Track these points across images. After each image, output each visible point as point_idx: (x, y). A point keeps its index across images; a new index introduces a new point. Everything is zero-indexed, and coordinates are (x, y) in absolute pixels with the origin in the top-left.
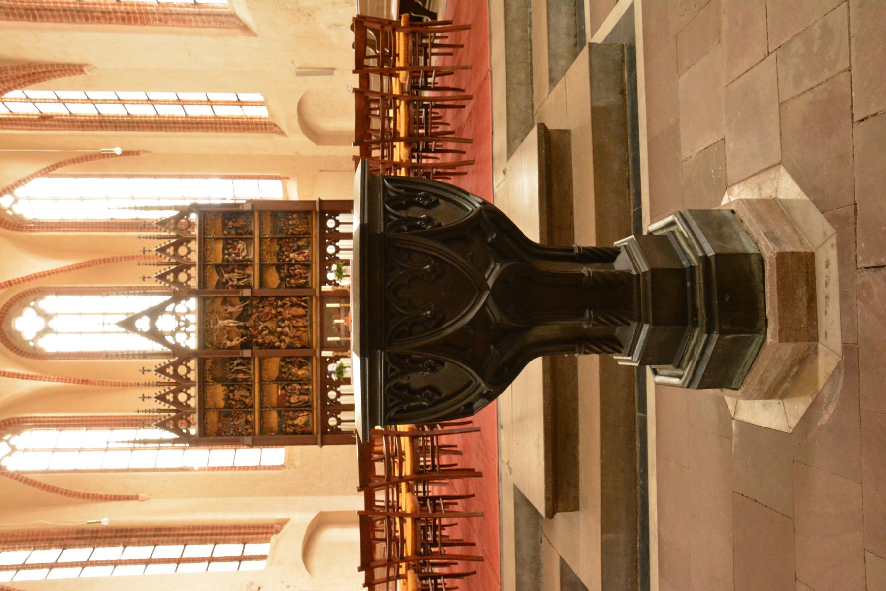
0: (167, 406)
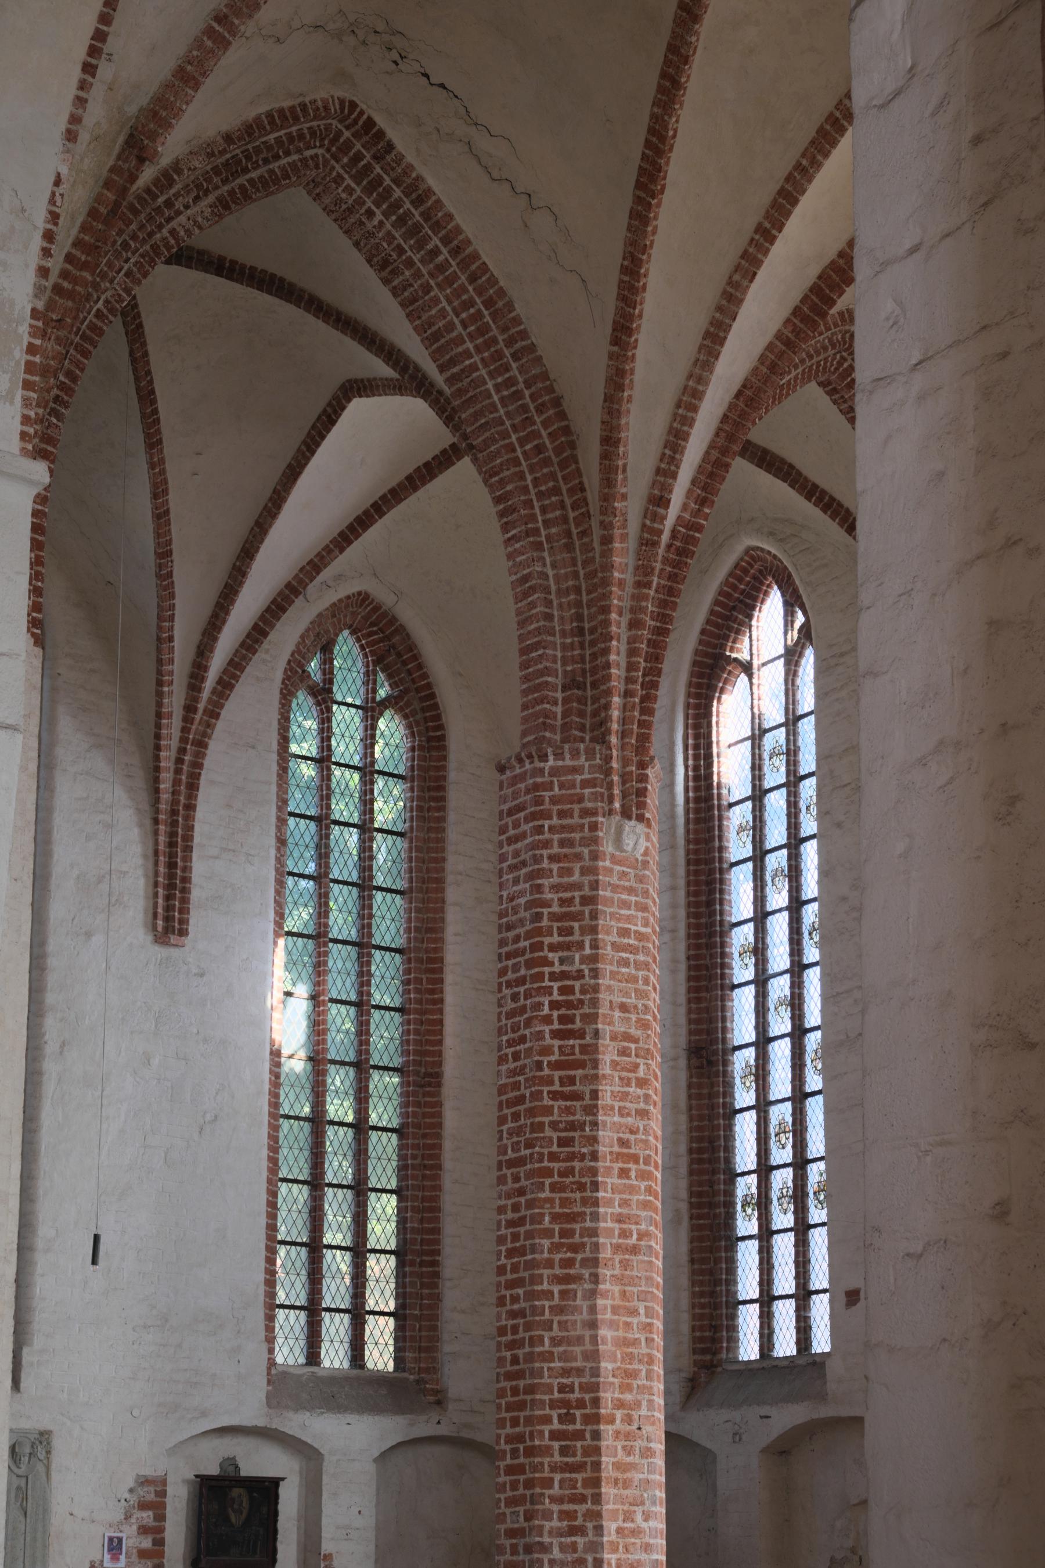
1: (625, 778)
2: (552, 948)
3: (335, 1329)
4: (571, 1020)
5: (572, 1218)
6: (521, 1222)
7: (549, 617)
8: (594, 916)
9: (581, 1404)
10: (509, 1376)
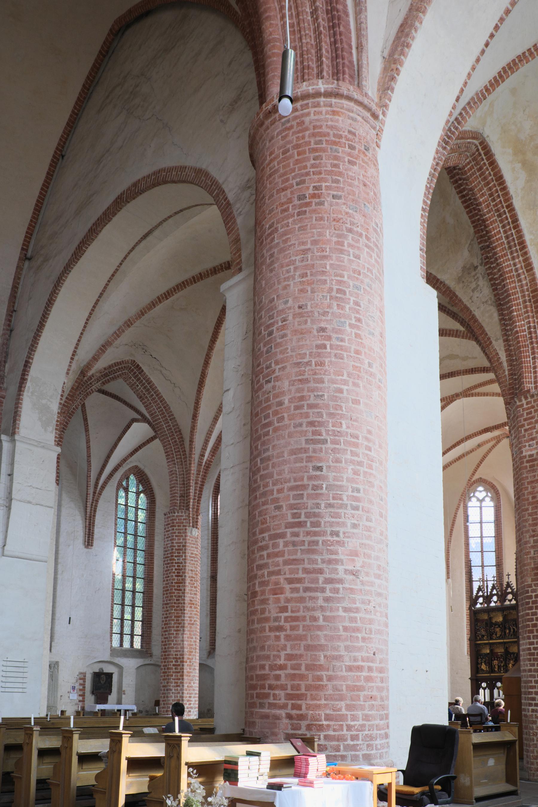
0: (489, 590)
1: (193, 518)
2: (176, 556)
3: (127, 639)
4: (179, 573)
5: (179, 617)
6: (167, 617)
7: (177, 480)
8: (185, 550)
9: (180, 658)
10: (164, 652)
